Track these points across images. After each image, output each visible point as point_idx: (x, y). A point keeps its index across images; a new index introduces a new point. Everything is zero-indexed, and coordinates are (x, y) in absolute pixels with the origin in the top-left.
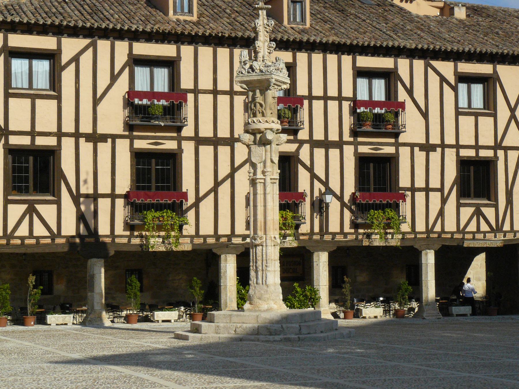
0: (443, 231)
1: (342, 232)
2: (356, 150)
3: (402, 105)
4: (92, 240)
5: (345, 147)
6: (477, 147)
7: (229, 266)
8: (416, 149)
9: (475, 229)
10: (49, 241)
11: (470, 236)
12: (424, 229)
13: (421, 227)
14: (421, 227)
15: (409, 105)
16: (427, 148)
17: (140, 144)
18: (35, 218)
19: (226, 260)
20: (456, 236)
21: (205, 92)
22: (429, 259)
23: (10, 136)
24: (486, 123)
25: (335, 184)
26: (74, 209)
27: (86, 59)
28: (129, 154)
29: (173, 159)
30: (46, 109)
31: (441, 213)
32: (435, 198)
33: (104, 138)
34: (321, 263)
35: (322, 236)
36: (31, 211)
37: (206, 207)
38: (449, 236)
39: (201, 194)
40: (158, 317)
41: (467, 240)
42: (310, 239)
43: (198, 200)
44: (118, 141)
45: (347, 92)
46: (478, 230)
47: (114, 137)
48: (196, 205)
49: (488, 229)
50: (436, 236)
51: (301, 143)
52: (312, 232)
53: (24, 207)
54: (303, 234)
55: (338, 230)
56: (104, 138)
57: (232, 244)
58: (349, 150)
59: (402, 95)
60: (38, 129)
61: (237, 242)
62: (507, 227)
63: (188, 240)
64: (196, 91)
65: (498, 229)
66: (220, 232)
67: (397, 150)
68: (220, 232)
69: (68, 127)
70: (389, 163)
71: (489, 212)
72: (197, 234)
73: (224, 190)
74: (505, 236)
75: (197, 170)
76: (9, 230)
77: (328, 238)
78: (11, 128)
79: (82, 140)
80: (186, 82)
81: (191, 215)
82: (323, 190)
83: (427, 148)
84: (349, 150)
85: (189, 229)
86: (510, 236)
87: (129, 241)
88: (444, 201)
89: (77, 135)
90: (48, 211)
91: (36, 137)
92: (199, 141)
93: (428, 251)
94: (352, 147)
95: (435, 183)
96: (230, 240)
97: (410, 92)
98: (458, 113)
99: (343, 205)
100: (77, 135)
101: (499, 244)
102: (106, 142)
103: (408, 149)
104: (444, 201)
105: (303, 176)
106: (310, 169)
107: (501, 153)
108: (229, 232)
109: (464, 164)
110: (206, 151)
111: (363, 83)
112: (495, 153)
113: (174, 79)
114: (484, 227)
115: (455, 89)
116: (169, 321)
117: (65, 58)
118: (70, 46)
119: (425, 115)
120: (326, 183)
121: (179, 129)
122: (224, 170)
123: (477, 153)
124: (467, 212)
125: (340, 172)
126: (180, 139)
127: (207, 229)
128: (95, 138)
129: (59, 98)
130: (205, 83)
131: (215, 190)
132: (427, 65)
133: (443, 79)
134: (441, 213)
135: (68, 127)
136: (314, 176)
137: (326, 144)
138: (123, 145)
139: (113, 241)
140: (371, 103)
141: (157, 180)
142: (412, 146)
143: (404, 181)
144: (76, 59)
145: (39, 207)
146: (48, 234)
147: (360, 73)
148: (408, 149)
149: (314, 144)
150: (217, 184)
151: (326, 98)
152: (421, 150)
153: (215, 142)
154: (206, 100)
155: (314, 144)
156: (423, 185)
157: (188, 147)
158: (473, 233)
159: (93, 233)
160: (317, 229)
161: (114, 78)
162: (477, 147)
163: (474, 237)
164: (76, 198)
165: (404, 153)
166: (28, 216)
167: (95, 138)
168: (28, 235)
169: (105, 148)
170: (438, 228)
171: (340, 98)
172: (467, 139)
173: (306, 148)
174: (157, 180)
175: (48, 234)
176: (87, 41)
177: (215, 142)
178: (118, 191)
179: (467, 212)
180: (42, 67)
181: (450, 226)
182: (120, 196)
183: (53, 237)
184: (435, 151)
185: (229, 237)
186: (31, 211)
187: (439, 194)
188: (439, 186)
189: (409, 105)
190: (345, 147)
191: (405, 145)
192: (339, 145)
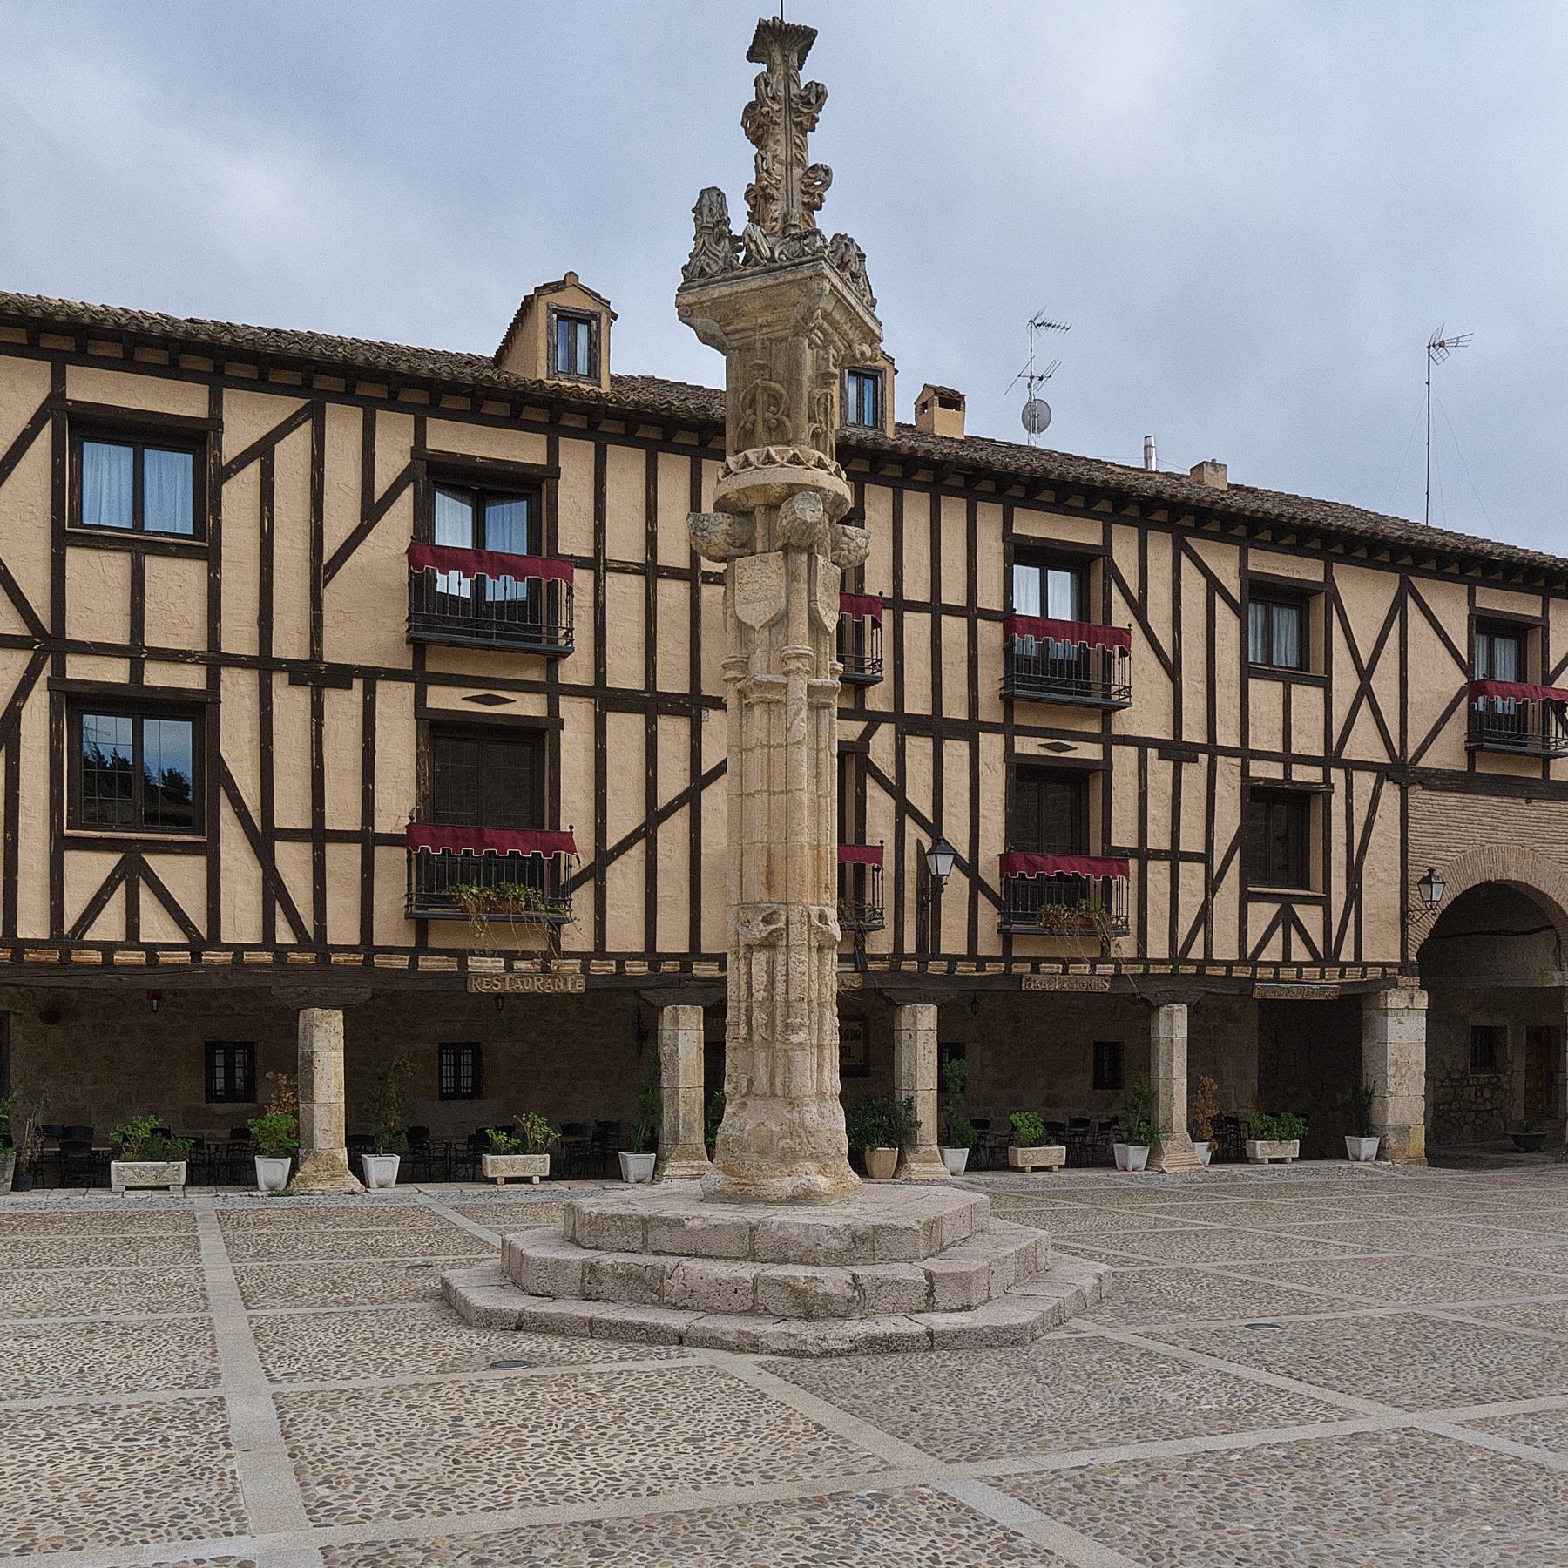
0: (1208, 960)
1: (972, 954)
2: (1009, 746)
3: (1123, 636)
4: (309, 958)
5: (983, 737)
6: (1287, 758)
7: (684, 1035)
8: (1152, 753)
9: (1278, 957)
10: (184, 957)
11: (1268, 973)
12: (1164, 953)
13: (1158, 947)
14: (1158, 947)
15: (1138, 641)
16: (1177, 752)
17: (444, 699)
18: (146, 897)
19: (676, 1021)
20: (1238, 972)
21: (623, 568)
22: (1175, 1025)
23: (69, 658)
24: (1307, 698)
25: (956, 830)
26: (256, 873)
27: (293, 453)
28: (412, 724)
29: (538, 739)
30: (175, 587)
31: (1204, 917)
32: (1192, 874)
33: (341, 676)
34: (921, 1028)
35: (923, 964)
36: (132, 873)
37: (624, 878)
38: (1222, 972)
39: (612, 841)
40: (494, 1169)
41: (1261, 981)
42: (895, 969)
43: (604, 857)
44: (382, 687)
45: (989, 598)
46: (1287, 960)
47: (372, 676)
48: (596, 873)
49: (1309, 958)
50: (1192, 970)
51: (874, 720)
52: (898, 952)
53: (111, 860)
54: (873, 958)
55: (962, 950)
56: (341, 676)
57: (694, 978)
58: (992, 746)
59: (1121, 616)
60: (152, 639)
61: (707, 974)
62: (1346, 955)
63: (575, 965)
64: (598, 564)
65: (1326, 958)
66: (661, 947)
67: (1107, 753)
68: (661, 947)
69: (239, 637)
70: (1082, 783)
71: (1310, 917)
72: (600, 951)
73: (673, 831)
74: (1342, 975)
75: (598, 775)
76: (68, 925)
77: (936, 967)
78: (74, 632)
79: (279, 680)
80: (574, 538)
81: (582, 899)
82: (927, 844)
83: (1177, 752)
84: (992, 746)
85: (577, 937)
86: (1352, 975)
87: (414, 963)
88: (1212, 884)
89: (264, 664)
90: (180, 874)
91: (147, 664)
92: (607, 699)
93: (1176, 1007)
94: (999, 740)
95: (1192, 841)
96: (686, 967)
97: (1139, 608)
98: (1248, 672)
99: (977, 885)
100: (264, 664)
101: (1331, 994)
102: (349, 687)
103: (1132, 752)
104: (1212, 884)
105: (879, 805)
106: (896, 790)
107: (1338, 776)
108: (684, 948)
109: (1255, 794)
110: (625, 729)
111: (1027, 577)
112: (1327, 776)
113: (542, 527)
114: (1300, 953)
115: (1239, 610)
116: (528, 1180)
117: (231, 447)
118: (245, 420)
119: (1173, 670)
120: (934, 828)
121: (554, 659)
122: (672, 783)
123: (1287, 772)
124: (1262, 914)
125: (971, 798)
126: (553, 690)
127: (625, 934)
128: (318, 676)
129: (212, 556)
130: (624, 543)
131: (647, 833)
132: (1180, 548)
133: (1214, 586)
134: (1204, 917)
135: (239, 637)
136: (904, 809)
137: (936, 728)
138: (395, 702)
139: (368, 961)
140: (1042, 626)
141: (488, 789)
142: (1143, 744)
143: (1123, 835)
144: (263, 451)
145: (1301, 911)
146: (178, 937)
147: (1021, 552)
148: (1132, 752)
149: (908, 725)
150: (655, 816)
151: (936, 608)
152: (293, 682)
153: (649, 703)
154: (625, 592)
155: (908, 725)
156: (1165, 845)
157: (576, 715)
158: (1275, 965)
159: (316, 941)
160: (910, 946)
161: (372, 511)
162: (136, 652)
163: (1276, 974)
164: (263, 840)
165: (1124, 758)
166: (122, 887)
167: (318, 676)
168: (122, 939)
169: (343, 706)
170: (1197, 953)
171: (971, 612)
172: (1265, 738)
173: (885, 733)
174: (488, 789)
175: (178, 937)
176: (297, 403)
177: (649, 703)
178: (382, 826)
179: (1262, 914)
180: (171, 475)
181: (1225, 948)
182: (391, 840)
183: (196, 946)
184: (1196, 761)
185: (685, 960)
186: (132, 873)
187: (1200, 868)
188: (1201, 849)
189: (1138, 641)
190: (983, 737)
191: (1126, 740)
192: (969, 730)
